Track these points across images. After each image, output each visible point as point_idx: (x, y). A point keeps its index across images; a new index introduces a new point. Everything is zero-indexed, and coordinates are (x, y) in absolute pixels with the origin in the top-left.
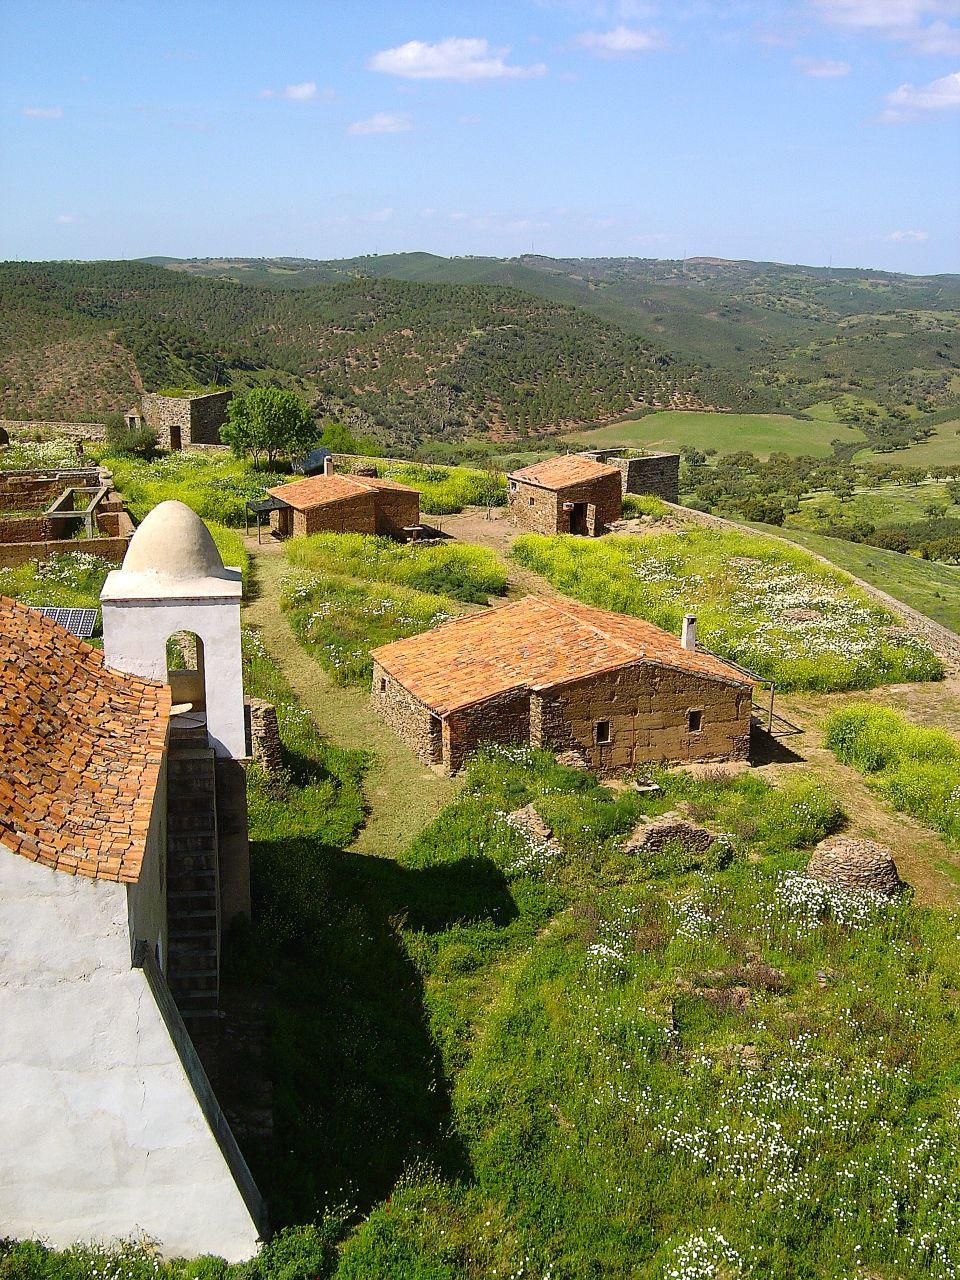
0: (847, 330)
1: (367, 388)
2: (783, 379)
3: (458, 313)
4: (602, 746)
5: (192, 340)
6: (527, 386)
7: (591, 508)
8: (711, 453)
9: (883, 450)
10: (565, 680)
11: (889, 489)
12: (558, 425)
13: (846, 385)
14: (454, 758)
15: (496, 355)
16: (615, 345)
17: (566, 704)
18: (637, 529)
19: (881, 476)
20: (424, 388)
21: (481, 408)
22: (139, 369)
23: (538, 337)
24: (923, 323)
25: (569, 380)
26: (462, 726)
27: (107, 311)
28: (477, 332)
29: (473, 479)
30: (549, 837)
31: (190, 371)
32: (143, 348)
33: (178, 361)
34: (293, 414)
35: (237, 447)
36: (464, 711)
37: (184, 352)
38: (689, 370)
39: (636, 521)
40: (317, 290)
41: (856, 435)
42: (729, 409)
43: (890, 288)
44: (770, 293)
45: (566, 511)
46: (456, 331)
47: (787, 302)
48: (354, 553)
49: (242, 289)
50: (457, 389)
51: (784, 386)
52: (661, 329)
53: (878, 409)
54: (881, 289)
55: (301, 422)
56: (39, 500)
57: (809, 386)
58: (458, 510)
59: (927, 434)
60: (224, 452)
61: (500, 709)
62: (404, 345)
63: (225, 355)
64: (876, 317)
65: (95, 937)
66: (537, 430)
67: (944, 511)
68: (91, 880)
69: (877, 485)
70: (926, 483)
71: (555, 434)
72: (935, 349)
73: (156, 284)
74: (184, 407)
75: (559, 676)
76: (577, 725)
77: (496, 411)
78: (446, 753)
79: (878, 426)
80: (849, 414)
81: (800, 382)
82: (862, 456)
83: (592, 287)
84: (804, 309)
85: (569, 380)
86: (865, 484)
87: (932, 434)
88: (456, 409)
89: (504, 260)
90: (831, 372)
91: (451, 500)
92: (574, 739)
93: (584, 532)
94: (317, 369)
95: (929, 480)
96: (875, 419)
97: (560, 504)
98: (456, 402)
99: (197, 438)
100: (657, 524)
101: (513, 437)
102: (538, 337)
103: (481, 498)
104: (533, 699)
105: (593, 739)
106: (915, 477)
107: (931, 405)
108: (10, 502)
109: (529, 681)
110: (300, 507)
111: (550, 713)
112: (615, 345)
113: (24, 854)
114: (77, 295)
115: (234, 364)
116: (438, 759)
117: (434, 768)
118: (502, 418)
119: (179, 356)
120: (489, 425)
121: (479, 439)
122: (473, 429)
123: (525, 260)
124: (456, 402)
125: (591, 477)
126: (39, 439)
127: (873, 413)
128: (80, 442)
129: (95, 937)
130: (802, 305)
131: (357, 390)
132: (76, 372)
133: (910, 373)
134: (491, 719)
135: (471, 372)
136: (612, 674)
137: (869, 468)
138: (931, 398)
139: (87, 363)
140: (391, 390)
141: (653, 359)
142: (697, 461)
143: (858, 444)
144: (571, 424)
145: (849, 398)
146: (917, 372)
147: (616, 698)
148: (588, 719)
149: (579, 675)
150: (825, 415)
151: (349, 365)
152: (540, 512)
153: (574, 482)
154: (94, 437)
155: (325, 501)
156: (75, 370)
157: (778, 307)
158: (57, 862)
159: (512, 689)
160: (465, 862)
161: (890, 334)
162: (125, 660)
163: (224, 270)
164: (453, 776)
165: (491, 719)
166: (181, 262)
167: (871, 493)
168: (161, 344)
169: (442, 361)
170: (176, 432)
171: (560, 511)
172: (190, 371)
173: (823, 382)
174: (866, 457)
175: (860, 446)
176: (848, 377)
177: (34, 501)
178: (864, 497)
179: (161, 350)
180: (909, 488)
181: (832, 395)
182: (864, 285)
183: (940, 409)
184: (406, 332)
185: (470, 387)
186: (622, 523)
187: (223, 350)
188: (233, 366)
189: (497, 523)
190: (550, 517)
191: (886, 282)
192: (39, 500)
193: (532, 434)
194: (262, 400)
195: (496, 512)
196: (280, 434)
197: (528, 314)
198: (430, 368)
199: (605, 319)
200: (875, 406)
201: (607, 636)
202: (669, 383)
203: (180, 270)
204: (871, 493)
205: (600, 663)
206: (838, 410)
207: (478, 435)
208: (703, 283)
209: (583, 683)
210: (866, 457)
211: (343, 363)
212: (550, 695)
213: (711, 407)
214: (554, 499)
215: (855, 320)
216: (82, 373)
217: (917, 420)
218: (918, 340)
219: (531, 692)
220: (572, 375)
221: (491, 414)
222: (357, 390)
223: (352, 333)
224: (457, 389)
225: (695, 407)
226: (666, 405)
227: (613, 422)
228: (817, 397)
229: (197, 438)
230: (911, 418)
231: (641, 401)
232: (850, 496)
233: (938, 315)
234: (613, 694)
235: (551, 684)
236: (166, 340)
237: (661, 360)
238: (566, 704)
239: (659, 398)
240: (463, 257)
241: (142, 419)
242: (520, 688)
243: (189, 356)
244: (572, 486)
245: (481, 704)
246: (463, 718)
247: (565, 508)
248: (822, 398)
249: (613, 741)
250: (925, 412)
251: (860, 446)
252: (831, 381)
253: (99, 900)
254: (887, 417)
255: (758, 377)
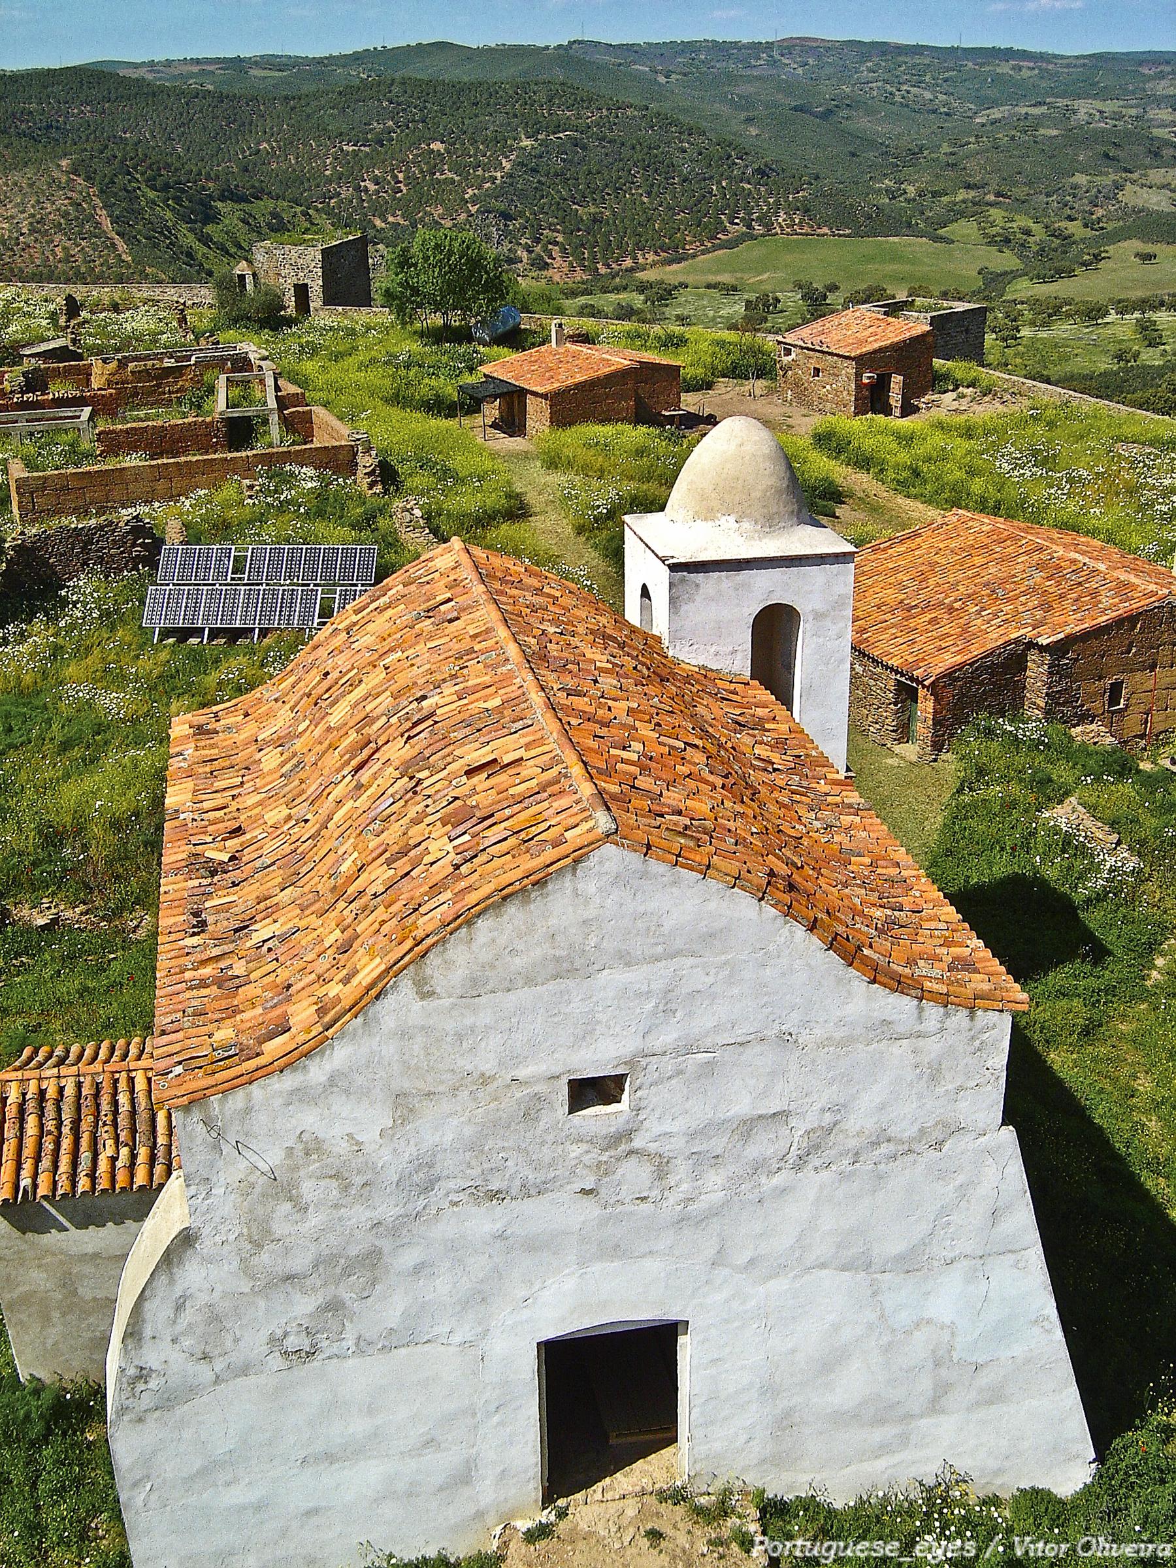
0: (989, 128)
1: (391, 219)
2: (911, 190)
3: (501, 118)
4: (1113, 712)
5: (168, 166)
6: (592, 209)
7: (897, 381)
8: (833, 288)
9: (1043, 279)
10: (1078, 629)
11: (1063, 329)
12: (635, 258)
13: (991, 198)
14: (937, 736)
15: (552, 171)
16: (700, 154)
17: (1077, 660)
18: (955, 405)
19: (1050, 312)
20: (463, 216)
21: (537, 241)
22: (105, 207)
23: (604, 147)
24: (1082, 116)
25: (645, 200)
26: (949, 694)
27: (54, 133)
28: (526, 143)
29: (721, 344)
30: (1119, 843)
31: (168, 206)
32: (107, 180)
33: (152, 195)
34: (475, 264)
35: (400, 311)
36: (950, 675)
37: (158, 184)
38: (797, 183)
39: (953, 395)
40: (316, 96)
41: (1006, 261)
42: (848, 231)
43: (1036, 71)
44: (886, 82)
45: (865, 384)
46: (500, 143)
47: (908, 92)
48: (640, 452)
49: (221, 98)
50: (506, 216)
51: (914, 200)
52: (754, 131)
53: (1034, 227)
54: (1025, 73)
55: (487, 273)
56: (170, 392)
57: (945, 199)
58: (709, 386)
59: (1097, 258)
60: (380, 315)
61: (992, 669)
62: (434, 162)
63: (210, 185)
64: (1023, 110)
65: (960, 1088)
66: (609, 266)
67: (1136, 356)
68: (966, 1012)
69: (1046, 324)
70: (1106, 320)
71: (632, 270)
72: (1100, 149)
73: (113, 97)
74: (313, 257)
75: (1066, 624)
76: (1089, 687)
77: (556, 243)
78: (923, 728)
79: (1035, 248)
80: (999, 234)
81: (934, 194)
82: (1018, 287)
83: (662, 79)
84: (931, 100)
85: (645, 200)
86: (1033, 323)
87: (1104, 258)
88: (506, 243)
89: (547, 48)
90: (971, 181)
91: (700, 371)
92: (1083, 706)
93: (887, 411)
94: (326, 197)
95: (1112, 317)
96: (1031, 239)
97: (858, 375)
98: (506, 233)
99: (331, 299)
100: (987, 399)
101: (580, 275)
102: (604, 147)
103: (735, 367)
104: (1033, 655)
105: (1104, 705)
106: (1094, 313)
107: (1099, 220)
108: (132, 396)
109: (1027, 632)
110: (540, 389)
111: (1057, 674)
112: (700, 154)
113: (880, 983)
114: (13, 114)
115: (223, 196)
116: (904, 732)
117: (897, 749)
118: (564, 250)
119: (153, 188)
120: (549, 261)
121: (537, 279)
122: (529, 267)
123: (574, 47)
124: (506, 233)
125: (896, 340)
126: (116, 308)
127: (1028, 232)
128: (183, 310)
129: (960, 1088)
130: (928, 95)
131: (378, 223)
132: (26, 215)
133: (1071, 180)
134: (981, 684)
135: (522, 195)
136: (1131, 619)
137: (1034, 303)
138: (1100, 212)
139: (38, 202)
140: (422, 220)
141: (750, 171)
142: (817, 299)
143: (1012, 271)
144: (651, 257)
145: (996, 214)
146: (1081, 179)
147: (1134, 650)
148: (1100, 679)
149: (1094, 622)
150: (968, 235)
151: (366, 190)
152: (828, 387)
153: (876, 346)
154: (189, 303)
155: (570, 381)
156: (23, 212)
157: (898, 99)
158: (922, 989)
159: (1008, 643)
160: (1015, 882)
161: (1042, 131)
162: (695, 647)
163: (192, 75)
164: (935, 760)
165: (981, 684)
166: (136, 66)
167: (1041, 335)
168: (129, 173)
169: (484, 180)
170: (302, 291)
171: (859, 386)
172: (168, 206)
173: (962, 195)
174: (1023, 288)
175: (1014, 275)
176: (993, 186)
177: (165, 394)
178: (1034, 339)
179: (130, 182)
180: (1087, 327)
181: (976, 209)
182: (1005, 69)
183: (1110, 226)
184: (437, 146)
185: (521, 214)
186: (933, 397)
187: (208, 178)
188: (222, 199)
189: (763, 401)
190: (845, 393)
191: (1031, 65)
192: (170, 392)
193: (603, 270)
194: (437, 246)
195: (760, 385)
196: (463, 291)
197: (590, 117)
198: (469, 191)
199: (684, 119)
200: (1030, 224)
201: (1102, 567)
202: (771, 200)
203: (134, 76)
204: (1041, 335)
205: (1136, 605)
206: (984, 229)
207: (534, 274)
208: (800, 71)
209: (1098, 632)
210: (1023, 288)
211: (358, 189)
212: (1058, 649)
213: (825, 230)
214: (850, 369)
215: (996, 114)
216: (32, 216)
217: (1083, 240)
218: (1078, 137)
219: (1031, 645)
220: (649, 194)
221: (550, 247)
222: (378, 223)
223: (367, 149)
224: (506, 216)
225: (806, 229)
226: (768, 226)
227: (703, 253)
228: (957, 213)
229: (331, 299)
230: (1076, 237)
231: (737, 224)
232: (1016, 339)
233: (1099, 105)
234: (1131, 645)
235: (1061, 636)
236: (135, 168)
237: (759, 171)
238: (1077, 660)
239: (759, 220)
240: (493, 45)
241: (254, 275)
242: (1017, 641)
243: (166, 187)
244: (875, 352)
245: (971, 665)
246: (950, 685)
247: (866, 381)
248: (962, 214)
249: (1127, 706)
250: (1092, 229)
251: (1014, 275)
252: (972, 193)
253: (973, 1038)
254: (1044, 237)
255: (880, 189)
